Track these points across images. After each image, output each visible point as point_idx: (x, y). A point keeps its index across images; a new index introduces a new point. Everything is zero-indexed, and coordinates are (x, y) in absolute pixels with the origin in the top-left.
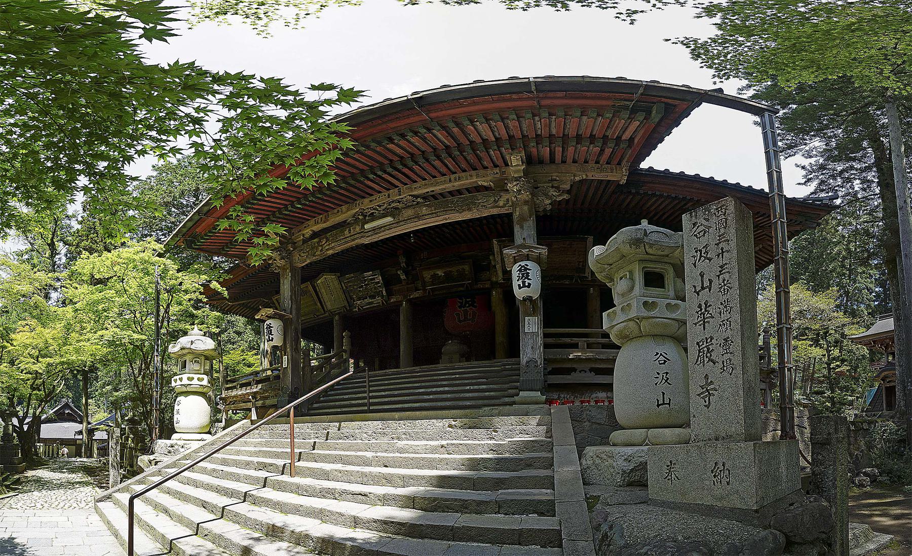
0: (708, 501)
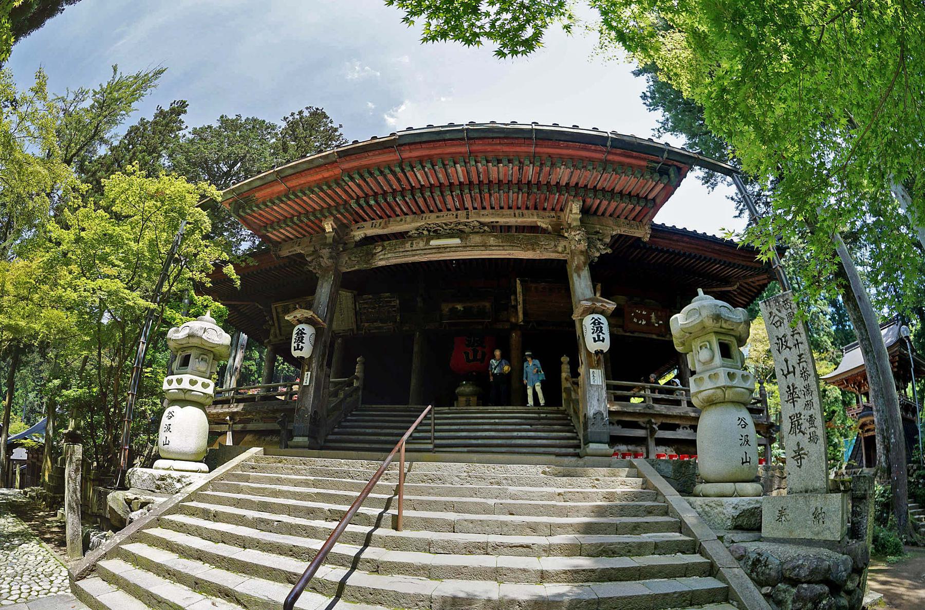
0: (809, 536)
